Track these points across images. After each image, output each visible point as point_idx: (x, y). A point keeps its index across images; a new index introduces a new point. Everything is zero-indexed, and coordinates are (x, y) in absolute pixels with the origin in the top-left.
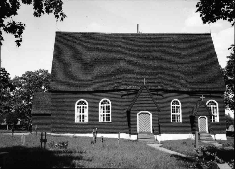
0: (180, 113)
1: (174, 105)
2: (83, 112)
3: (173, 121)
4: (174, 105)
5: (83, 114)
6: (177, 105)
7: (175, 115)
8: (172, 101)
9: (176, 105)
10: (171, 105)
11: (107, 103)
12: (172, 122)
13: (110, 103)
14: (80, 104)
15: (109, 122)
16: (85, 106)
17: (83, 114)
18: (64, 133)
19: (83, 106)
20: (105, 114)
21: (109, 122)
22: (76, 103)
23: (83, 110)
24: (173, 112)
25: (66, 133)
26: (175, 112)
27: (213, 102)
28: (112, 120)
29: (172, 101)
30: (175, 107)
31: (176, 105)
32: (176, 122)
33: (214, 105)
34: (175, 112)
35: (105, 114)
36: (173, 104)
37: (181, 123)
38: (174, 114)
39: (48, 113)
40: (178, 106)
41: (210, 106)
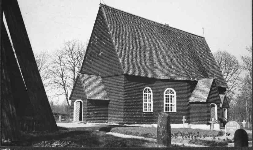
0: (175, 102)
1: (145, 94)
2: (171, 102)
3: (166, 110)
4: (167, 95)
5: (171, 103)
6: (149, 93)
7: (168, 105)
8: (144, 89)
9: (148, 93)
10: (165, 95)
11: (172, 92)
12: (144, 111)
13: (175, 92)
14: (168, 92)
15: (168, 112)
16: (173, 95)
17: (171, 103)
18: (135, 124)
19: (171, 95)
20: (170, 103)
21: (168, 112)
22: (165, 92)
23: (171, 99)
24: (166, 102)
25: (136, 124)
26: (168, 102)
27: (171, 91)
28: (153, 110)
29: (144, 89)
30: (168, 96)
31: (170, 95)
32: (170, 111)
33: (171, 94)
34: (168, 102)
35: (170, 103)
36: (166, 93)
37: (152, 113)
38: (167, 103)
39: (107, 99)
40: (173, 95)
41: (146, 94)
